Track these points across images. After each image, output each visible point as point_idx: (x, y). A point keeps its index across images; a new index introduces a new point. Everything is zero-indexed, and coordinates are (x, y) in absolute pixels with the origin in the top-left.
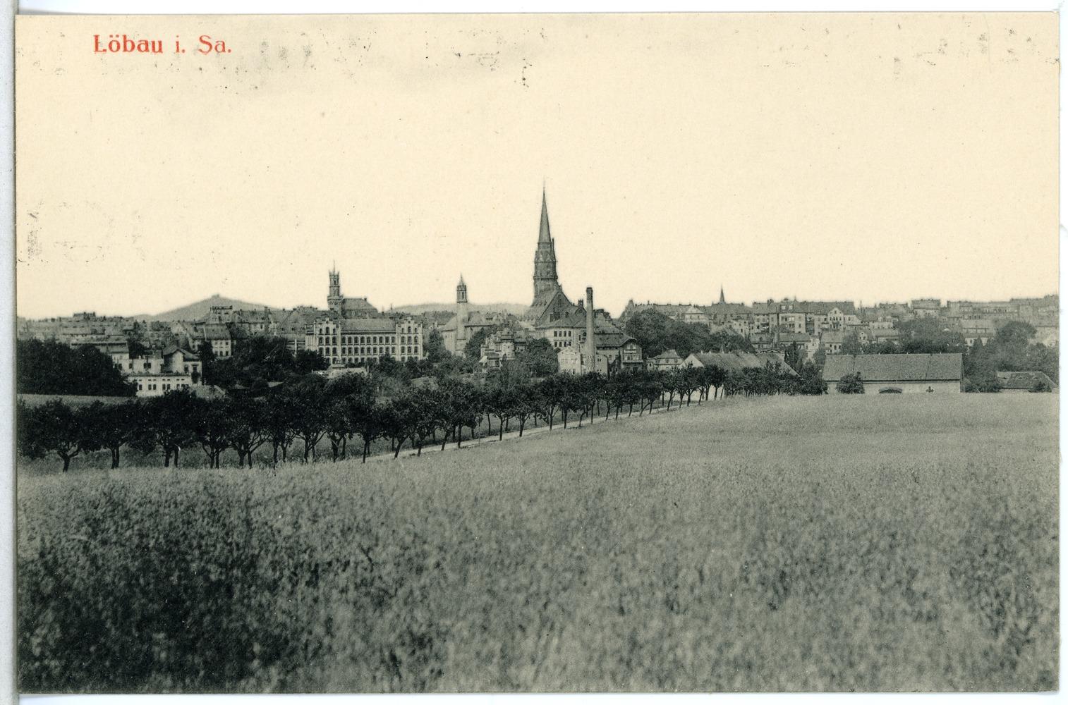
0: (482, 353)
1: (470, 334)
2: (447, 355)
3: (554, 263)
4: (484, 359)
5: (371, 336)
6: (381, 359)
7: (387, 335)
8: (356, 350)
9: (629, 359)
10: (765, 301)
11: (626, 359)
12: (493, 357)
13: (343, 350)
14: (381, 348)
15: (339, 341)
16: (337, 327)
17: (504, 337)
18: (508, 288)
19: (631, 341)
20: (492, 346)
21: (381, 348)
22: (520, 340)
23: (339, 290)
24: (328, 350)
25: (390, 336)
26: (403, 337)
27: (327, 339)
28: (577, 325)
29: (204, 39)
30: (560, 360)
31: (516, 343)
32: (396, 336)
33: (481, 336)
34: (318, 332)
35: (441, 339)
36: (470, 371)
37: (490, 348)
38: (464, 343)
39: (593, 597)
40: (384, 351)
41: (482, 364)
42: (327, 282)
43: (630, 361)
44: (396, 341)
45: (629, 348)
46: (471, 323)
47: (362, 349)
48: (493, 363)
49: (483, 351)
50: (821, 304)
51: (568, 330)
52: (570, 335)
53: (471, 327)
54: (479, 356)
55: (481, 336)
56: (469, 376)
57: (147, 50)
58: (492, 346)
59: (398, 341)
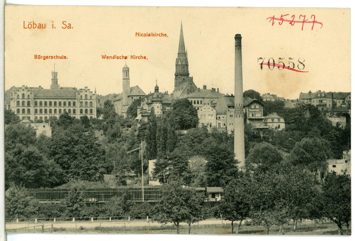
0: (138, 113)
1: (130, 102)
2: (115, 115)
3: (187, 65)
4: (139, 117)
5: (48, 101)
6: (61, 117)
7: (69, 100)
8: (46, 111)
9: (253, 115)
10: (308, 92)
11: (251, 115)
12: (146, 114)
13: (36, 111)
14: (60, 110)
15: (32, 105)
16: (31, 94)
17: (154, 99)
18: (156, 78)
19: (255, 102)
20: (146, 107)
21: (60, 110)
22: (167, 102)
23: (57, 82)
24: (70, 110)
25: (72, 101)
26: (82, 102)
27: (23, 102)
28: (207, 96)
29: (64, 23)
30: (199, 116)
31: (163, 104)
32: (76, 101)
33: (138, 102)
34: (16, 97)
35: (113, 106)
36: (129, 126)
37: (144, 108)
38: (127, 107)
39: (198, 153)
40: (62, 112)
41: (137, 120)
42: (51, 77)
43: (254, 118)
44: (76, 105)
45: (253, 107)
46: (131, 94)
47: (55, 110)
48: (146, 120)
49: (139, 111)
50: (340, 94)
51: (200, 100)
52: (201, 103)
53: (132, 96)
54: (136, 115)
55: (138, 102)
56: (128, 130)
57: (40, 28)
58: (146, 107)
59: (78, 104)
